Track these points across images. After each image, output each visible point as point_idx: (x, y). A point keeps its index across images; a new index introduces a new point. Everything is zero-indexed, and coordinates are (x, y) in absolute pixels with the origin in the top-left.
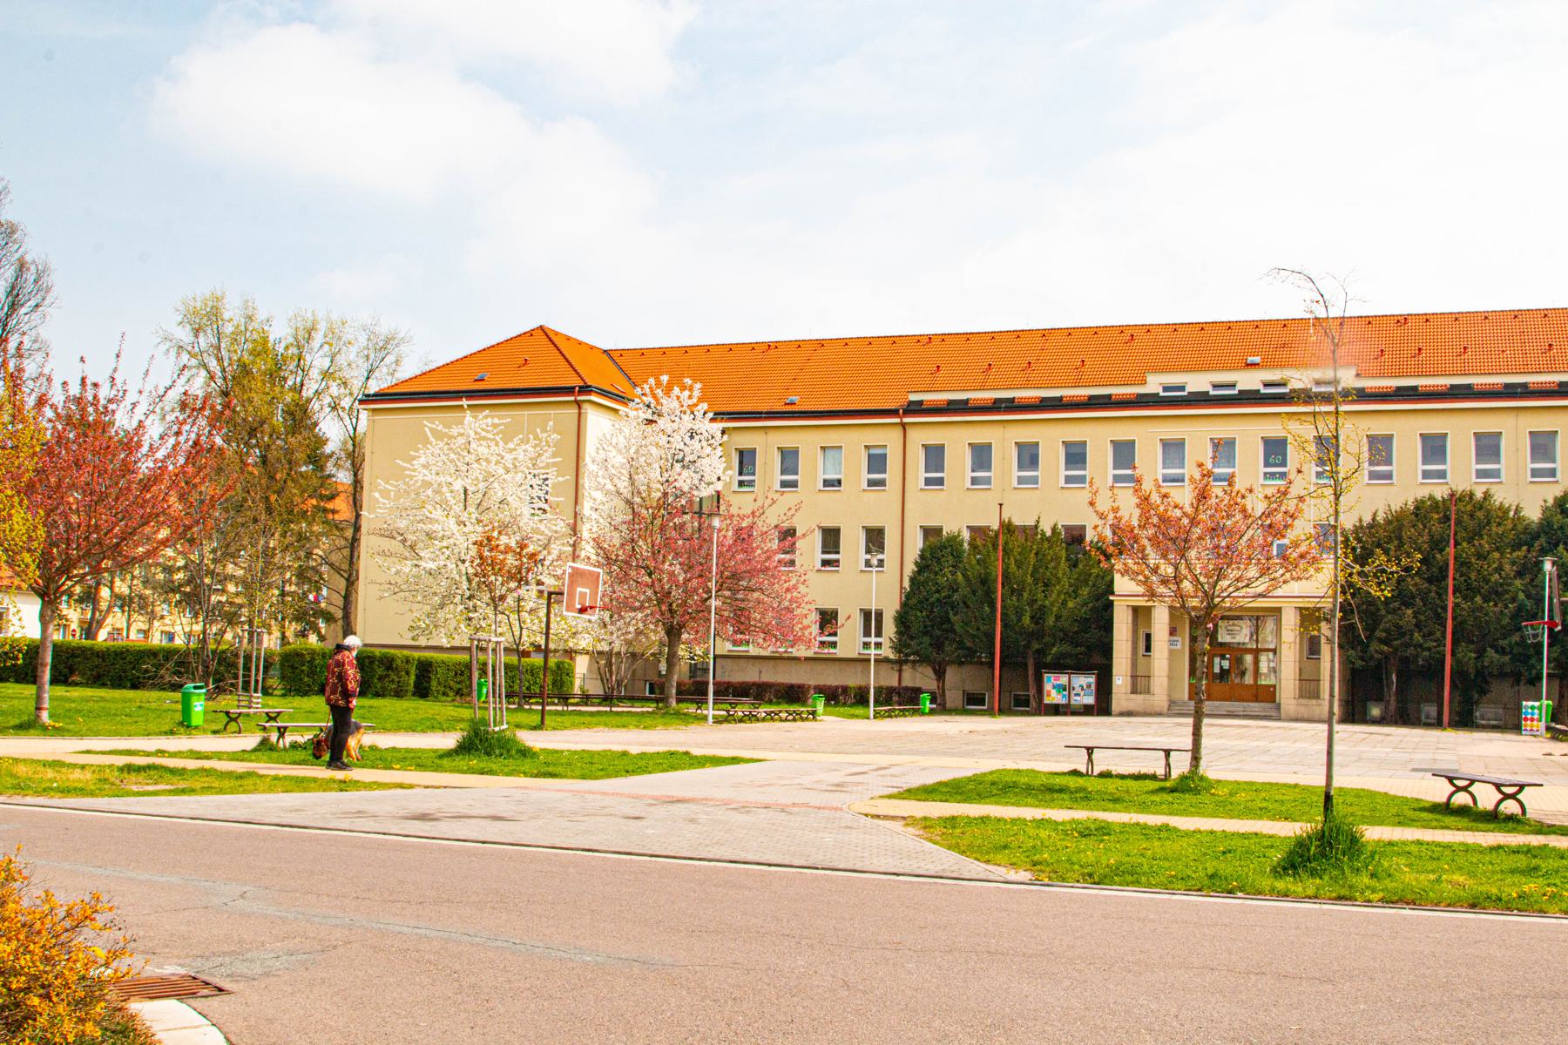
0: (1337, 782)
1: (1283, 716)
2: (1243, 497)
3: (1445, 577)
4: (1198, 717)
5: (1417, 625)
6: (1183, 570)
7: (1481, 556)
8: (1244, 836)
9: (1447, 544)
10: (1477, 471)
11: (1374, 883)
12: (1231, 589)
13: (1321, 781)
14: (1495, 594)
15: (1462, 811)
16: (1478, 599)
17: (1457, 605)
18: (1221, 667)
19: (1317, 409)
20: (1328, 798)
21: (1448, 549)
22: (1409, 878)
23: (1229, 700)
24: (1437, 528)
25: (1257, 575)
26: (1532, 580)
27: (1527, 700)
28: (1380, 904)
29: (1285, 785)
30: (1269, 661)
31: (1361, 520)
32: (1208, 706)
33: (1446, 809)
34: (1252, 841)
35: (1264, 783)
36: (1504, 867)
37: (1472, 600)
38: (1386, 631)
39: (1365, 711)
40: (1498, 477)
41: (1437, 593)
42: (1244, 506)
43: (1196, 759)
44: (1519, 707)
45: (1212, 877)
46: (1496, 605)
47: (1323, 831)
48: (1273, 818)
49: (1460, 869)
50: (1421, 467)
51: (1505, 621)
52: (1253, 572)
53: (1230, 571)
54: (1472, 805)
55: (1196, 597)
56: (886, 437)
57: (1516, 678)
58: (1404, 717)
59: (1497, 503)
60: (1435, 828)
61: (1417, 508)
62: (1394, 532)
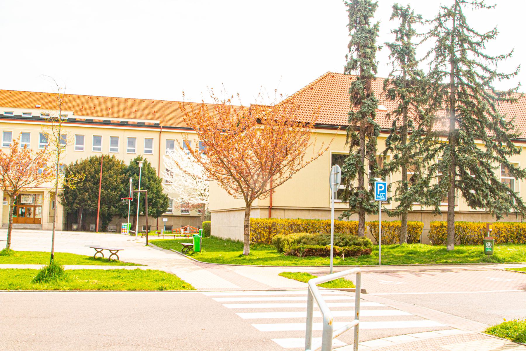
0: (55, 251)
1: (43, 229)
2: (29, 153)
3: (99, 183)
4: (10, 228)
5: (89, 198)
6: (6, 177)
7: (110, 176)
8: (24, 270)
9: (100, 172)
10: (76, 147)
11: (67, 284)
12: (23, 184)
13: (50, 251)
14: (115, 189)
15: (99, 259)
16: (109, 190)
17: (102, 192)
18: (22, 212)
19: (53, 124)
20: (52, 256)
21: (100, 174)
22: (79, 281)
23: (25, 223)
24: (97, 167)
25: (33, 180)
26: (126, 185)
27: (123, 223)
28: (68, 291)
29: (41, 252)
30: (39, 210)
31: (72, 163)
32: (14, 225)
33: (94, 258)
34: (27, 272)
35: (33, 252)
36: (110, 276)
37: (107, 190)
38: (79, 200)
39: (71, 227)
40: (117, 151)
41: (96, 188)
42: (29, 156)
43: (9, 244)
44: (121, 225)
45: (10, 285)
46: (114, 192)
47: (50, 266)
48: (35, 264)
49: (96, 278)
50: (3, 142)
51: (117, 197)
52: (31, 179)
53: (23, 178)
54: (102, 256)
55: (11, 187)
56: (153, 135)
57: (120, 216)
58: (84, 228)
59: (117, 160)
60: (90, 265)
61: (91, 160)
62: (83, 167)
